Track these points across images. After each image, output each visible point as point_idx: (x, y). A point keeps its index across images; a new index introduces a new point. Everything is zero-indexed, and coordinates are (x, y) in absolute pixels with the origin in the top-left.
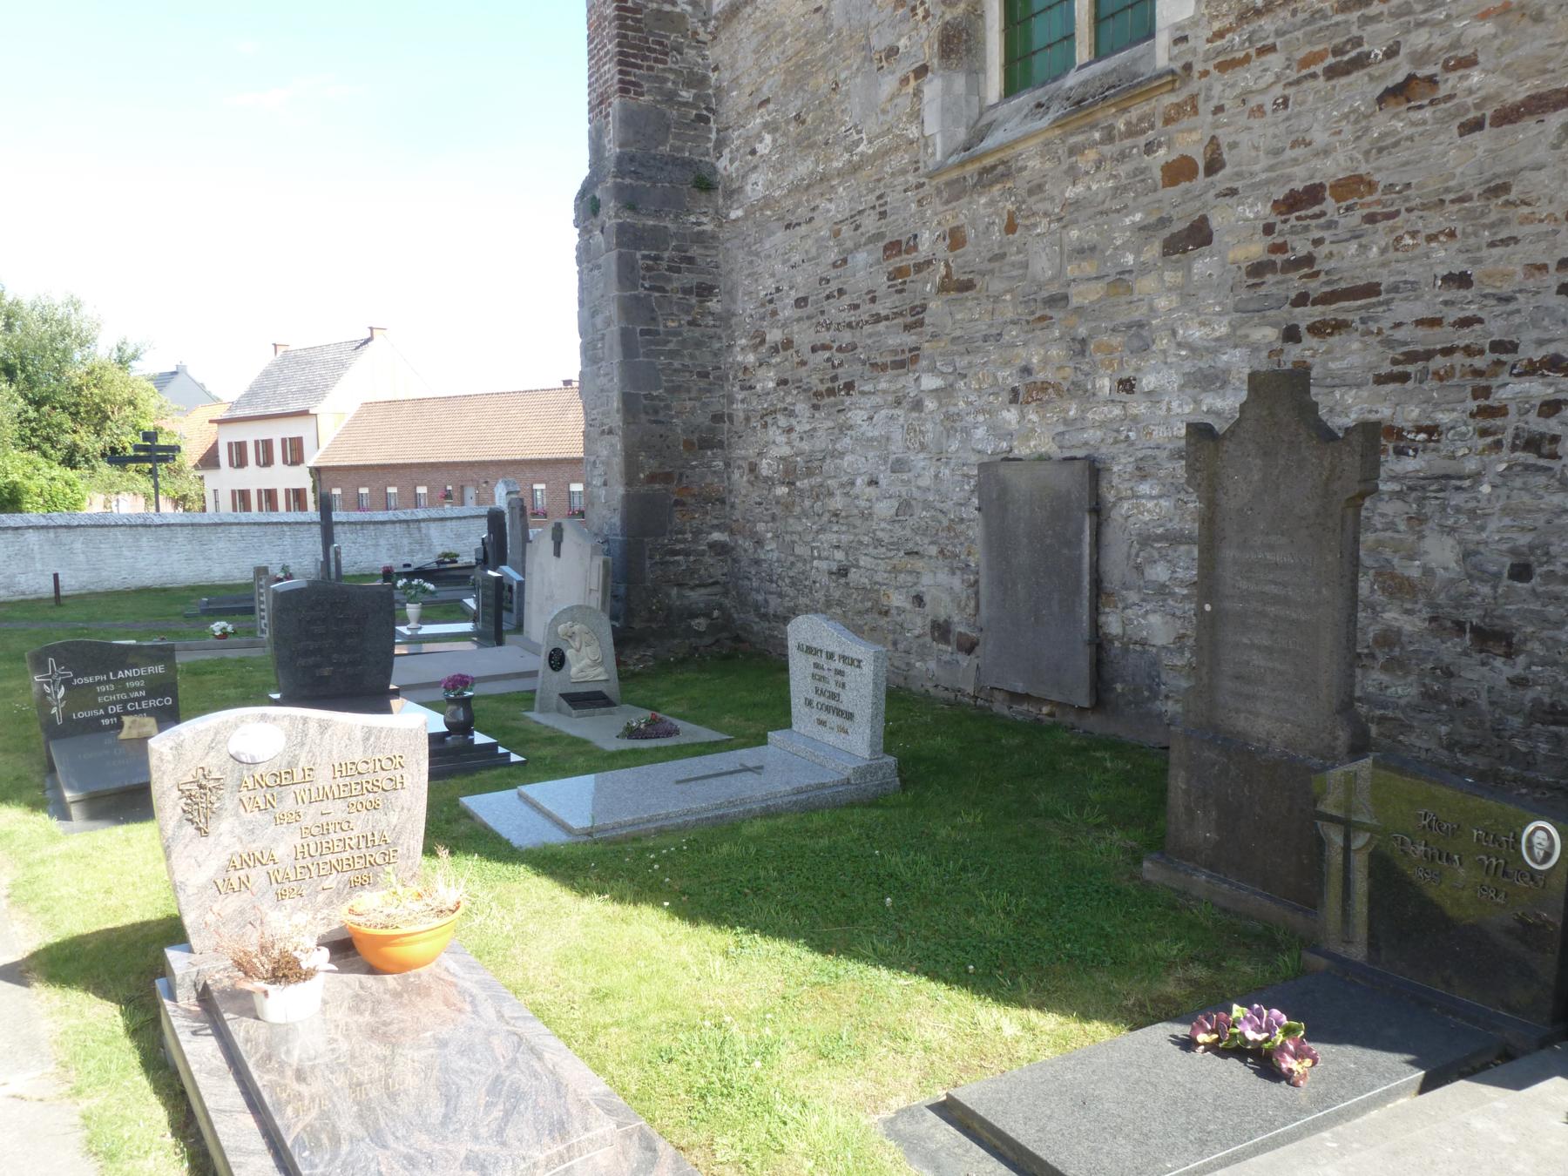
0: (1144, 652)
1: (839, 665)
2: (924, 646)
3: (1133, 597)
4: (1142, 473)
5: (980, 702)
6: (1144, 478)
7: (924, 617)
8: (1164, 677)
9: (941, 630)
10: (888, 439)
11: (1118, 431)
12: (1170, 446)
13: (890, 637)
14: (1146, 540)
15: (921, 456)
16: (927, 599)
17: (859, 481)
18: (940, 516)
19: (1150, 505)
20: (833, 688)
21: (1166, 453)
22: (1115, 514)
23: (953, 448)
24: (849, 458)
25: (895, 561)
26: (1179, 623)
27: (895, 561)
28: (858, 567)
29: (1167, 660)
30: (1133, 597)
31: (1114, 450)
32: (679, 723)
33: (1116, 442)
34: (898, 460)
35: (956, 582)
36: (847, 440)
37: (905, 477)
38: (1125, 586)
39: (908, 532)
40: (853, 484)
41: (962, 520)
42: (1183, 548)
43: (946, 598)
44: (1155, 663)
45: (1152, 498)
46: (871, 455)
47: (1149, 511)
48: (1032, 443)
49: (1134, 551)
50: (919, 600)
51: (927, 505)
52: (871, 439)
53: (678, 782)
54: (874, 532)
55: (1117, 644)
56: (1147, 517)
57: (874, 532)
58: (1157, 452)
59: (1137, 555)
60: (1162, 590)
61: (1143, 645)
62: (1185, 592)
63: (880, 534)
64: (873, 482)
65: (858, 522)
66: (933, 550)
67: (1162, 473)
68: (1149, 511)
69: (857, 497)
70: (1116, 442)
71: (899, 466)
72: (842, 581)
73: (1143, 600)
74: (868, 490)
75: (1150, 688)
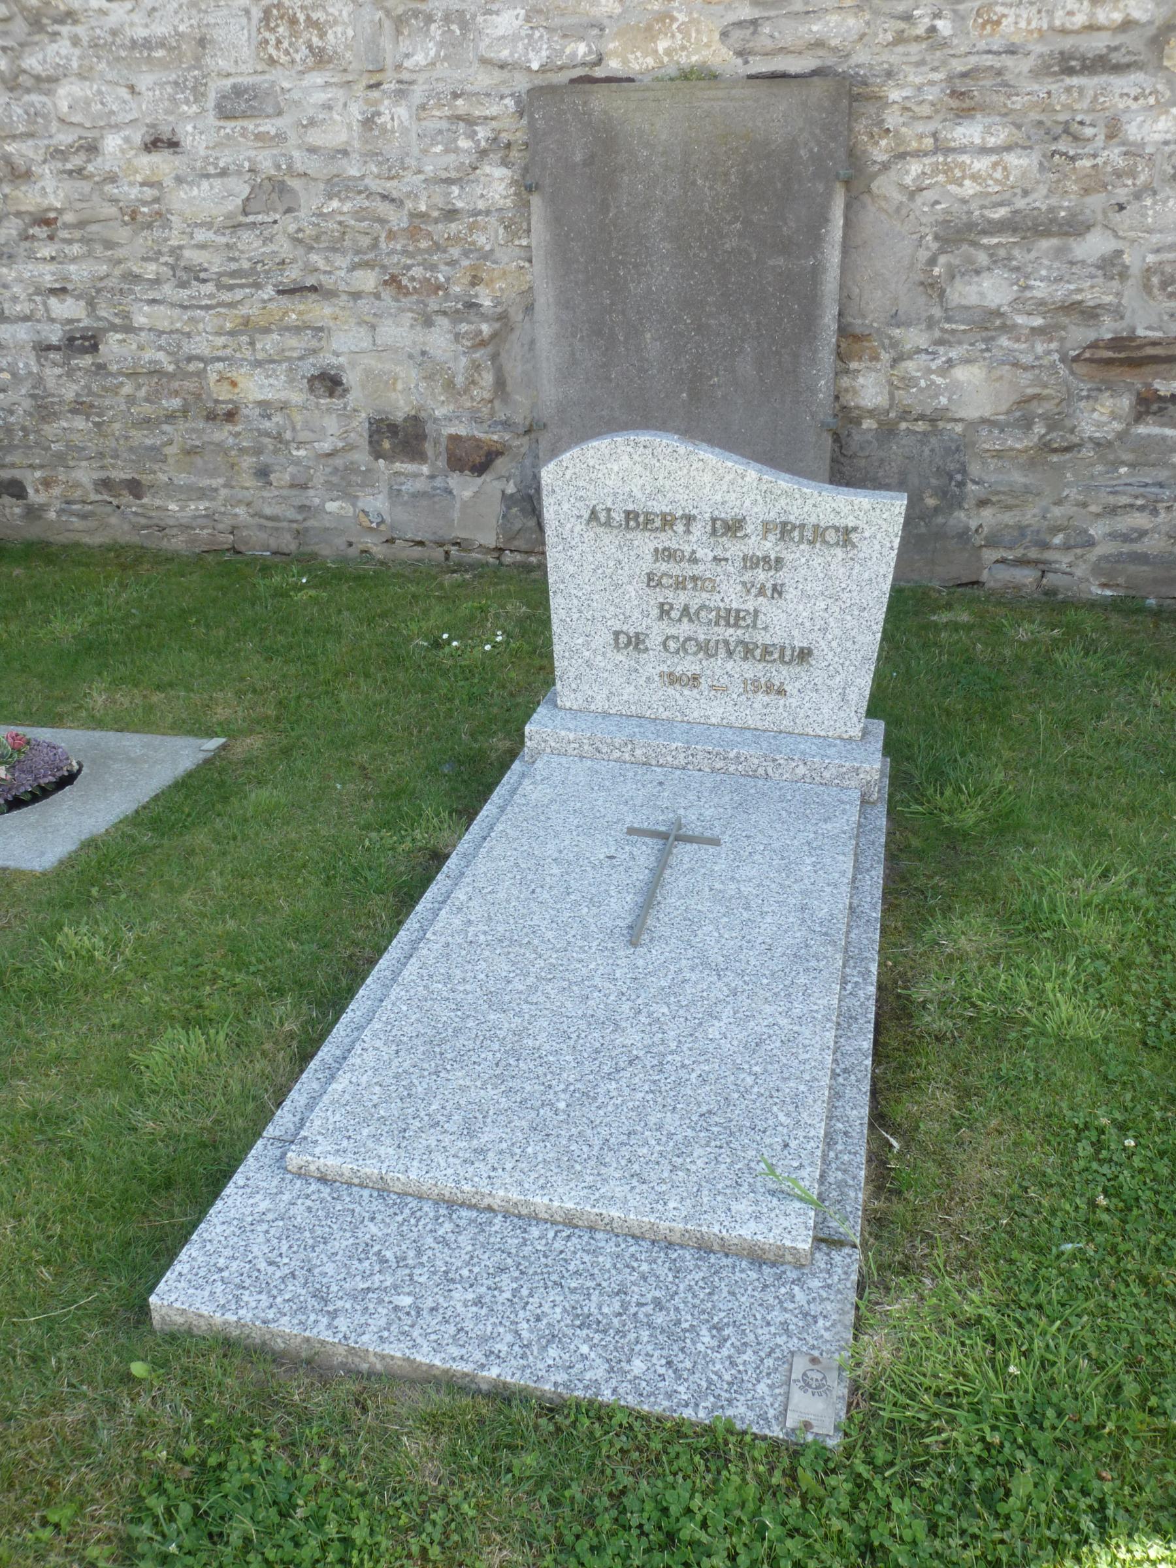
0: (936, 432)
1: (756, 544)
2: (351, 468)
3: (915, 337)
4: (962, 100)
5: (508, 558)
6: (964, 113)
7: (346, 415)
8: (975, 469)
9: (400, 437)
10: (202, 42)
11: (908, 18)
12: (1039, 48)
13: (248, 462)
14: (958, 233)
15: (317, 78)
16: (351, 378)
17: (112, 143)
18: (383, 208)
19: (981, 164)
20: (731, 596)
21: (1026, 65)
22: (884, 186)
23: (420, 58)
24: (66, 94)
25: (244, 310)
26: (1025, 378)
27: (244, 310)
28: (128, 329)
29: (989, 441)
30: (915, 337)
31: (894, 57)
32: (67, 741)
33: (900, 39)
34: (238, 91)
35: (440, 341)
36: (63, 47)
37: (268, 127)
38: (895, 319)
39: (284, 248)
40: (92, 149)
41: (451, 214)
42: (1045, 244)
43: (409, 375)
44: (959, 448)
45: (984, 150)
46: (145, 81)
47: (974, 177)
48: (662, 45)
49: (923, 255)
50: (329, 383)
51: (337, 186)
52: (148, 44)
53: (635, 934)
54: (176, 251)
55: (868, 424)
56: (969, 188)
57: (176, 251)
58: (1008, 61)
59: (932, 261)
60: (989, 323)
61: (933, 421)
62: (1038, 322)
63: (192, 256)
64: (161, 142)
65: (122, 234)
66: (368, 280)
67: (1018, 102)
68: (974, 177)
69: (112, 179)
70: (900, 39)
71: (239, 104)
72: (86, 361)
73: (940, 342)
74: (147, 162)
75: (943, 493)
